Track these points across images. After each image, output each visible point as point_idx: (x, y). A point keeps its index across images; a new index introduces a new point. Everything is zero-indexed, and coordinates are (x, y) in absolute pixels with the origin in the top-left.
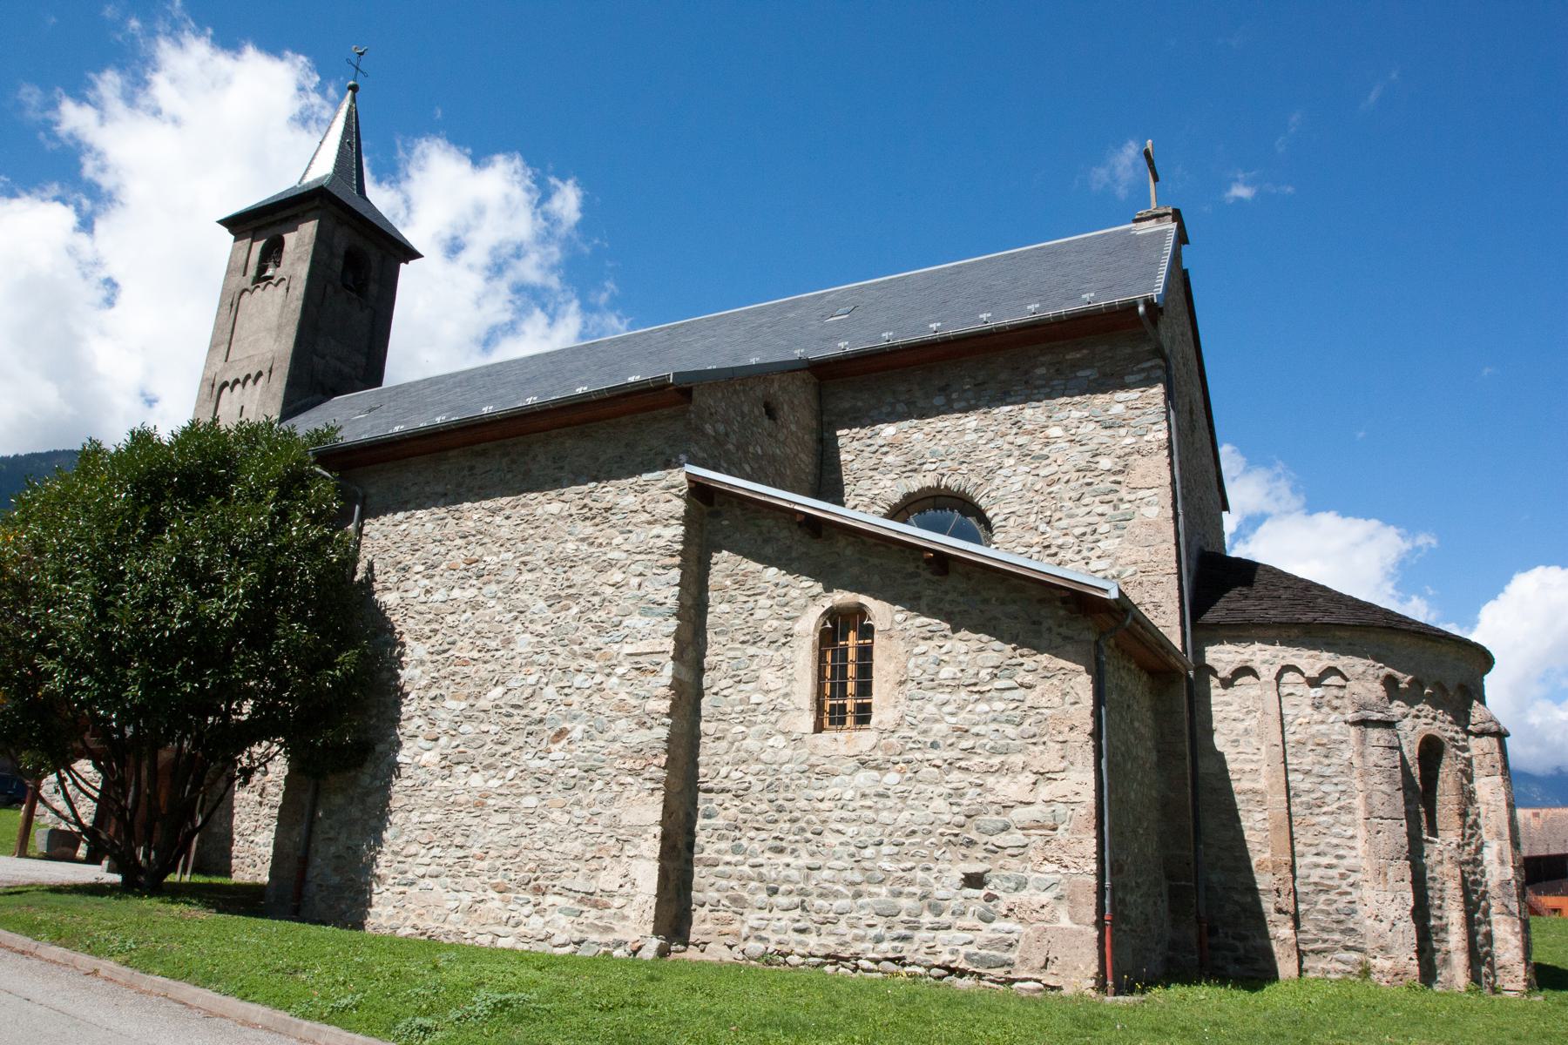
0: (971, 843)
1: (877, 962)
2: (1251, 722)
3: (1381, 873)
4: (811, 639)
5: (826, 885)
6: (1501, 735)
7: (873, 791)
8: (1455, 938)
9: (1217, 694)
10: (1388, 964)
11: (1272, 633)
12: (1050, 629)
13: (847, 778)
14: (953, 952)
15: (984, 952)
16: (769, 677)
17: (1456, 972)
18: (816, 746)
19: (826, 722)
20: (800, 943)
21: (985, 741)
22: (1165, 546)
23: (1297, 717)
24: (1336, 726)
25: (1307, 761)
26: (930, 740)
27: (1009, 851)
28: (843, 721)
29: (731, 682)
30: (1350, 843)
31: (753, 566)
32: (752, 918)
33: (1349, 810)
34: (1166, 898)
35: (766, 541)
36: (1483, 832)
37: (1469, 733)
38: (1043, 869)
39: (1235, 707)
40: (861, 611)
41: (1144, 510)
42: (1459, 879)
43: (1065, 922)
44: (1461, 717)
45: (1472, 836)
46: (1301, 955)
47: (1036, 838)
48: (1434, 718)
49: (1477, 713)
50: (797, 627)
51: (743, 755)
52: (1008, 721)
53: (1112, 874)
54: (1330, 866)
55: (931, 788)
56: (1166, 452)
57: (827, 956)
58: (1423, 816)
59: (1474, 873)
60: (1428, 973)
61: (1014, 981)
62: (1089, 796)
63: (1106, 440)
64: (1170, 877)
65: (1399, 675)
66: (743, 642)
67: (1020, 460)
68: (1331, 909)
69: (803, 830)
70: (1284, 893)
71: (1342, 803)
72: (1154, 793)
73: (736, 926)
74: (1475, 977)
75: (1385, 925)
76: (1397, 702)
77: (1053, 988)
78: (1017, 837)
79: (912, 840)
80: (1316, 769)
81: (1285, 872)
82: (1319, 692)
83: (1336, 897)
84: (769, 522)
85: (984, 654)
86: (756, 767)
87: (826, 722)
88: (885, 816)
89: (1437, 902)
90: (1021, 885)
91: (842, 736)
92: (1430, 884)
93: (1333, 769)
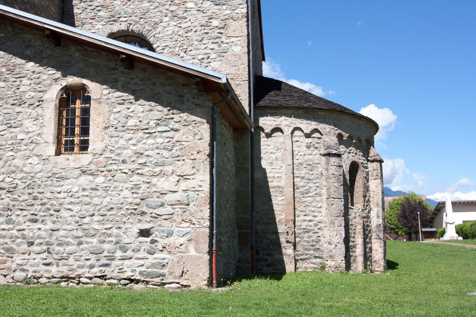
0: (143, 213)
1: (91, 278)
2: (279, 154)
3: (332, 223)
4: (54, 103)
5: (62, 239)
6: (381, 161)
7: (89, 187)
8: (359, 251)
9: (264, 141)
10: (333, 263)
11: (290, 112)
12: (188, 100)
13: (74, 180)
14: (132, 271)
15: (149, 270)
16: (28, 124)
17: (358, 265)
18: (56, 163)
19: (63, 150)
20: (46, 271)
21: (152, 159)
22: (243, 66)
23: (299, 151)
24: (316, 157)
25: (303, 172)
26: (121, 159)
27: (164, 217)
28: (72, 149)
29: (5, 127)
30: (319, 210)
31: (19, 61)
32: (18, 259)
33: (320, 195)
34: (237, 238)
35: (27, 47)
36: (371, 204)
37: (368, 161)
38: (181, 225)
39: (272, 147)
40: (83, 88)
41: (233, 48)
42: (362, 224)
43: (193, 252)
44: (366, 154)
45: (367, 206)
46: (296, 261)
47: (178, 210)
48: (356, 154)
49: (373, 152)
50: (46, 97)
51: (13, 168)
52: (164, 149)
53: (216, 227)
54: (310, 221)
55: (121, 185)
56: (245, 19)
57: (62, 277)
58: (350, 197)
59: (367, 222)
60: (348, 267)
61: (165, 284)
62: (206, 187)
63: (216, 11)
64: (239, 227)
65: (344, 133)
66: (13, 105)
67: (172, 19)
68: (310, 240)
69: (49, 209)
70: (290, 233)
71: (317, 192)
72: (234, 188)
73: (8, 264)
74: (365, 267)
75: (333, 246)
76: (342, 146)
77: (185, 286)
78: (168, 209)
79: (111, 213)
80: (307, 176)
81: (291, 224)
82: (310, 140)
83: (312, 235)
84: (29, 36)
85: (152, 113)
86: (21, 175)
87: (63, 150)
88: (96, 200)
89: (353, 235)
90: (170, 234)
91: (72, 157)
92: (351, 227)
93: (314, 176)
